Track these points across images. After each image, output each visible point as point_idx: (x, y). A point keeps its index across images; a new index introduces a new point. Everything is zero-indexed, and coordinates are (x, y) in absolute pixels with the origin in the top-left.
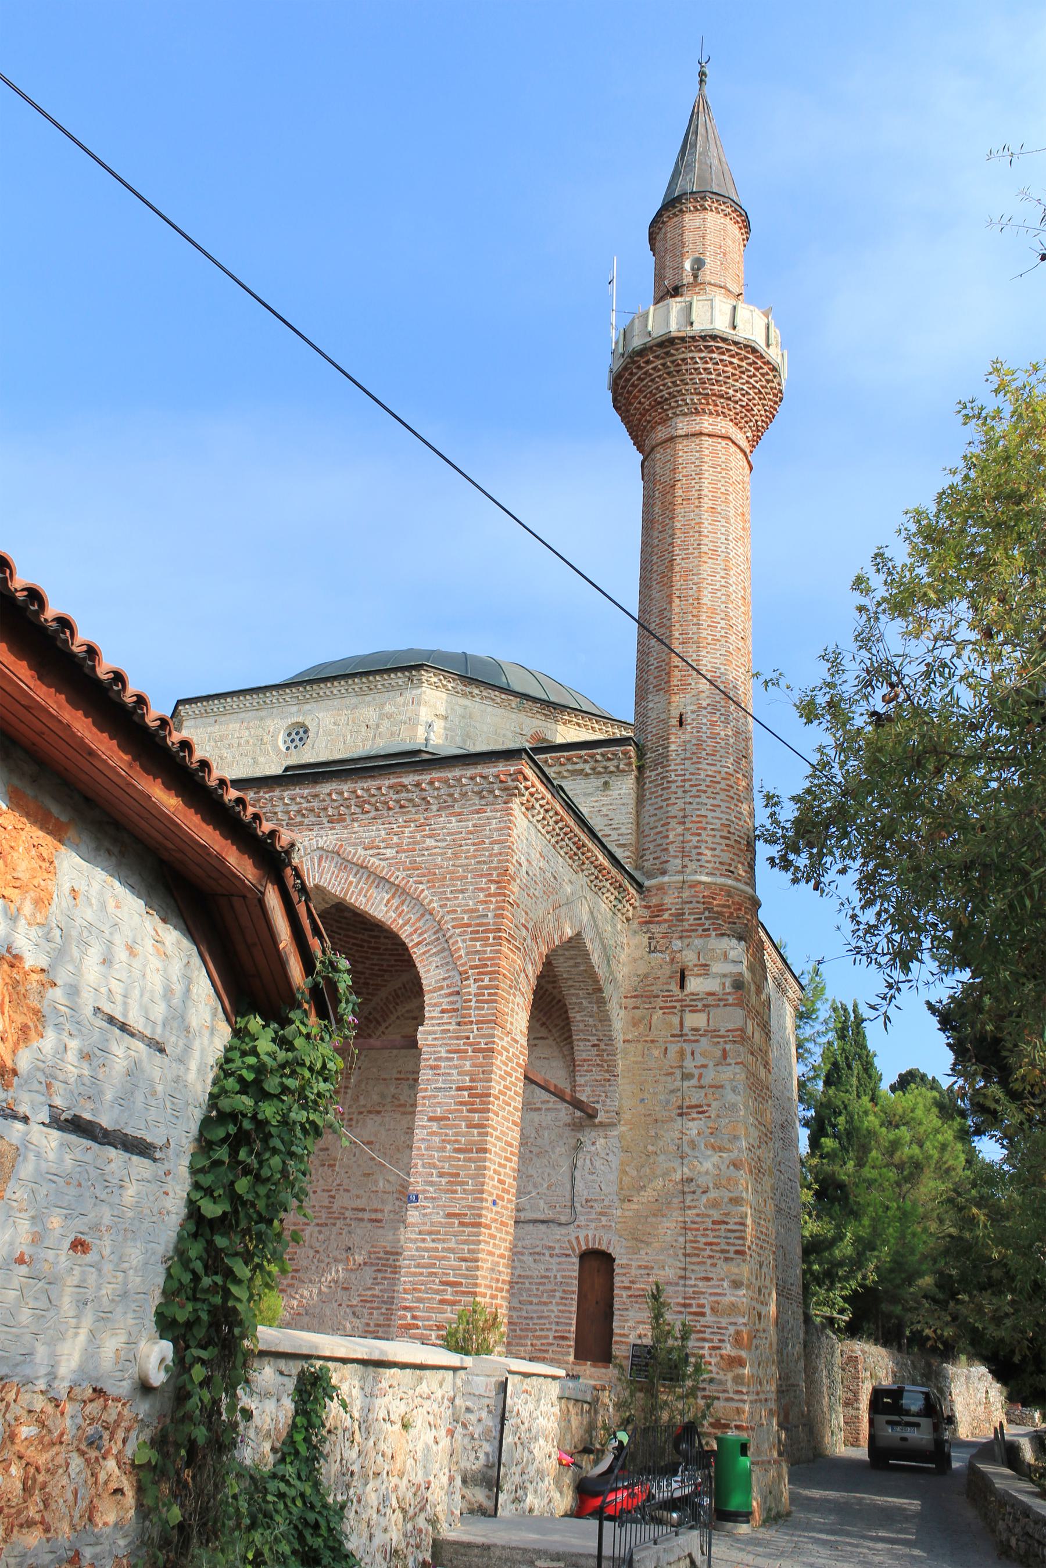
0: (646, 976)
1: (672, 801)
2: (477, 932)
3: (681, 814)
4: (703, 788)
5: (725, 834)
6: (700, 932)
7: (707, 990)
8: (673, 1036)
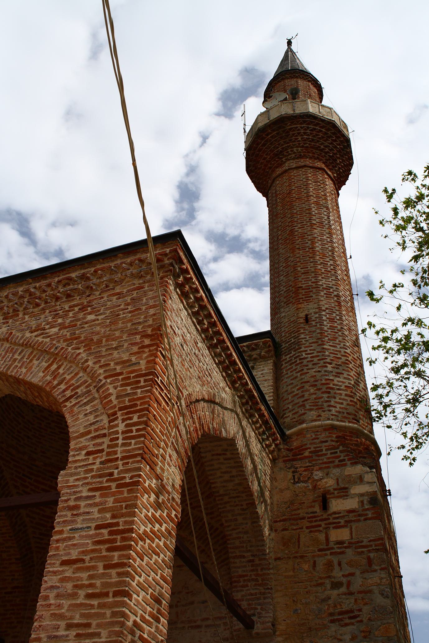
0: (292, 503)
1: (305, 371)
2: (129, 378)
3: (312, 379)
4: (328, 360)
5: (348, 393)
6: (337, 462)
7: (348, 508)
8: (320, 550)
